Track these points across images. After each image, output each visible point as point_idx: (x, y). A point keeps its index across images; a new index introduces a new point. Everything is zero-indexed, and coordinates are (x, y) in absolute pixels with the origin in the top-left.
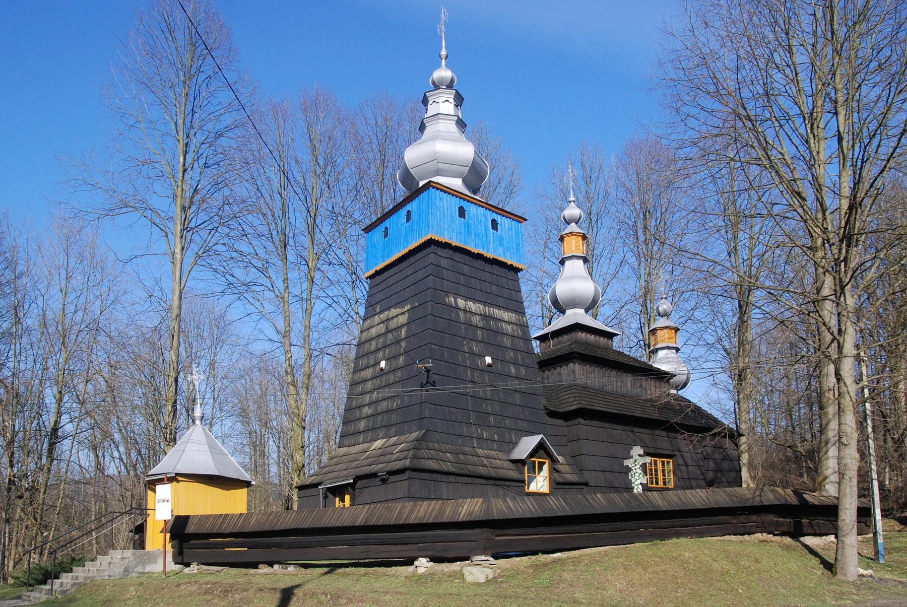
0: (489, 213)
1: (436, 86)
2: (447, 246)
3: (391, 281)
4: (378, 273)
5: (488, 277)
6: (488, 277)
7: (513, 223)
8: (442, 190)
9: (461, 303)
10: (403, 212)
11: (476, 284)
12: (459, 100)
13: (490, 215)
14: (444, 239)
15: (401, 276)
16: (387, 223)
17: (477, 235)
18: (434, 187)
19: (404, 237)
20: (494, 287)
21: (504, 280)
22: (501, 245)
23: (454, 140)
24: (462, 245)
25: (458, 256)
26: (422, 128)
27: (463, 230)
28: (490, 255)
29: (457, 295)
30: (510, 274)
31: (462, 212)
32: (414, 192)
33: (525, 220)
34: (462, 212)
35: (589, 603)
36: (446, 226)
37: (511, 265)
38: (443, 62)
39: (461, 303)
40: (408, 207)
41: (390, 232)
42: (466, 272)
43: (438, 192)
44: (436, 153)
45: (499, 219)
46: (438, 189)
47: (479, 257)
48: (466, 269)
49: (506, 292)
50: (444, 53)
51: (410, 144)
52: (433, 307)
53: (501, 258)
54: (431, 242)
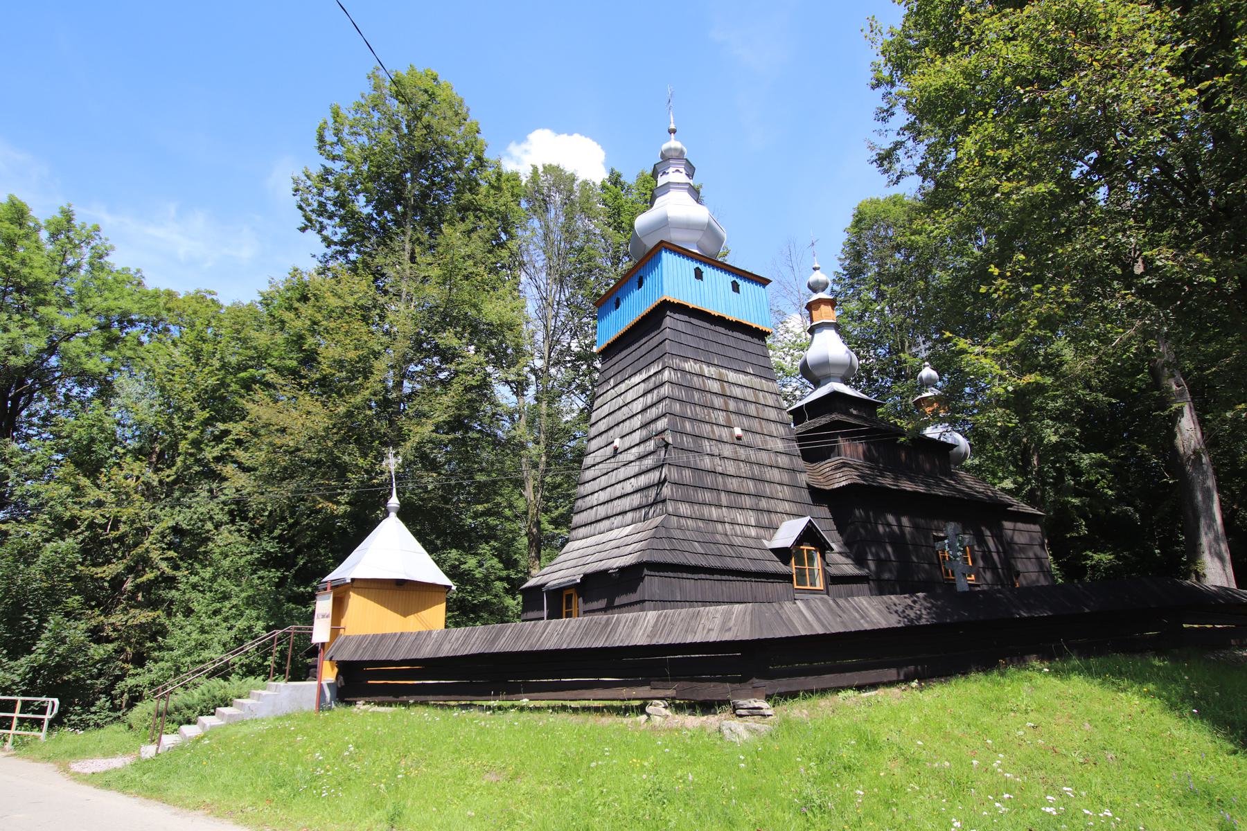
34: (699, 274)
44: (667, 218)
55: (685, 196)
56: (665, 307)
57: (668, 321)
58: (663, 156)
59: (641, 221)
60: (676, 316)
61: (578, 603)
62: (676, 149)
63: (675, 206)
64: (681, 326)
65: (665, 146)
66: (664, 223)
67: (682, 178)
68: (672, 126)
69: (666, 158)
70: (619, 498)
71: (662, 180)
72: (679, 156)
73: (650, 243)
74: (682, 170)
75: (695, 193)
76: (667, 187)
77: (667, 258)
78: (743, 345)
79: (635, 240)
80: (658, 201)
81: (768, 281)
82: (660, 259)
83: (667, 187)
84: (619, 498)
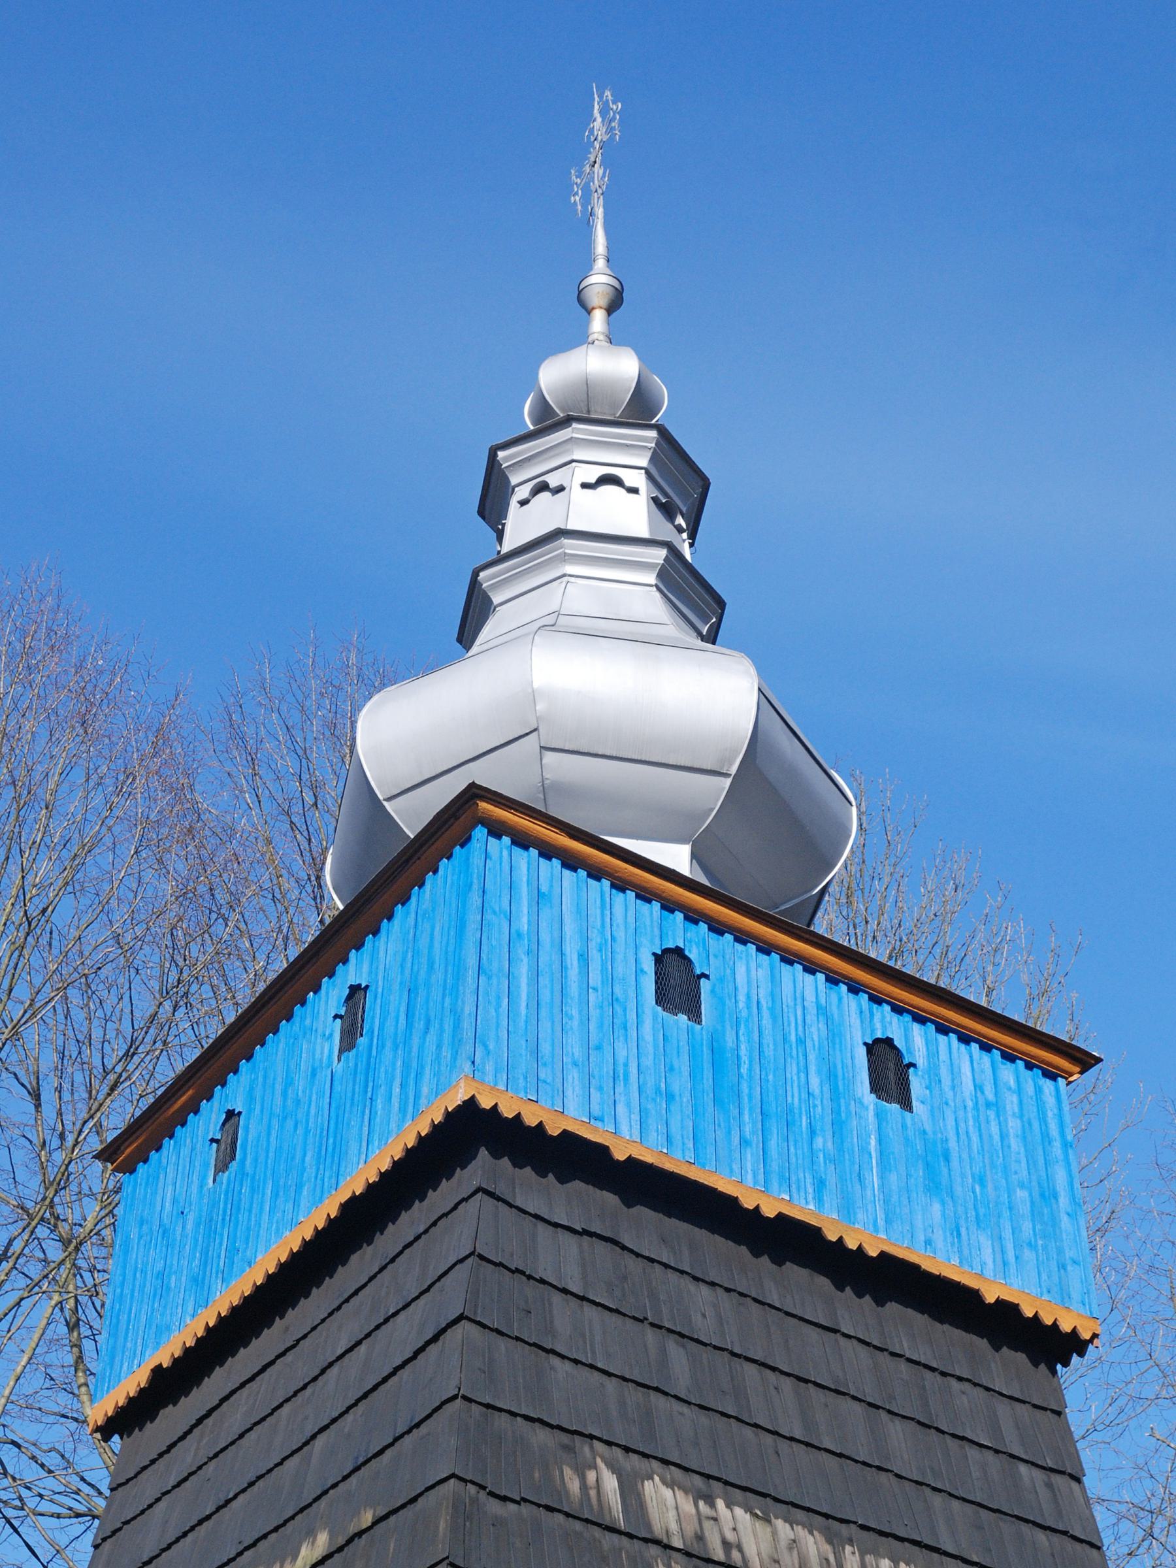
0: (852, 1006)
1: (549, 420)
2: (574, 1158)
3: (235, 1416)
4: (168, 1385)
5: (856, 1367)
6: (856, 1367)
7: (1010, 1073)
8: (547, 852)
9: (668, 1505)
10: (329, 998)
11: (783, 1406)
12: (681, 486)
13: (859, 1020)
14: (563, 1111)
15: (299, 1367)
16: (235, 1092)
17: (765, 1094)
18: (497, 830)
19: (322, 1124)
20: (896, 1431)
21: (965, 1398)
22: (934, 1186)
23: (639, 639)
24: (678, 1160)
25: (646, 1228)
26: (475, 611)
27: (680, 1084)
28: (865, 1231)
29: (640, 1454)
30: (1007, 1367)
31: (677, 983)
32: (394, 871)
33: (1085, 1061)
34: (677, 983)
35: (5, 734)
36: (575, 1048)
37: (1007, 1310)
38: (599, 316)
39: (668, 1505)
40: (354, 970)
41: (249, 1132)
42: (705, 1328)
43: (526, 859)
44: (533, 696)
45: (915, 1041)
46: (522, 841)
47: (791, 1241)
48: (703, 1310)
49: (979, 1473)
50: (599, 280)
51: (384, 686)
52: (463, 1514)
53: (941, 1260)
54: (470, 1132)
75: (697, 601)
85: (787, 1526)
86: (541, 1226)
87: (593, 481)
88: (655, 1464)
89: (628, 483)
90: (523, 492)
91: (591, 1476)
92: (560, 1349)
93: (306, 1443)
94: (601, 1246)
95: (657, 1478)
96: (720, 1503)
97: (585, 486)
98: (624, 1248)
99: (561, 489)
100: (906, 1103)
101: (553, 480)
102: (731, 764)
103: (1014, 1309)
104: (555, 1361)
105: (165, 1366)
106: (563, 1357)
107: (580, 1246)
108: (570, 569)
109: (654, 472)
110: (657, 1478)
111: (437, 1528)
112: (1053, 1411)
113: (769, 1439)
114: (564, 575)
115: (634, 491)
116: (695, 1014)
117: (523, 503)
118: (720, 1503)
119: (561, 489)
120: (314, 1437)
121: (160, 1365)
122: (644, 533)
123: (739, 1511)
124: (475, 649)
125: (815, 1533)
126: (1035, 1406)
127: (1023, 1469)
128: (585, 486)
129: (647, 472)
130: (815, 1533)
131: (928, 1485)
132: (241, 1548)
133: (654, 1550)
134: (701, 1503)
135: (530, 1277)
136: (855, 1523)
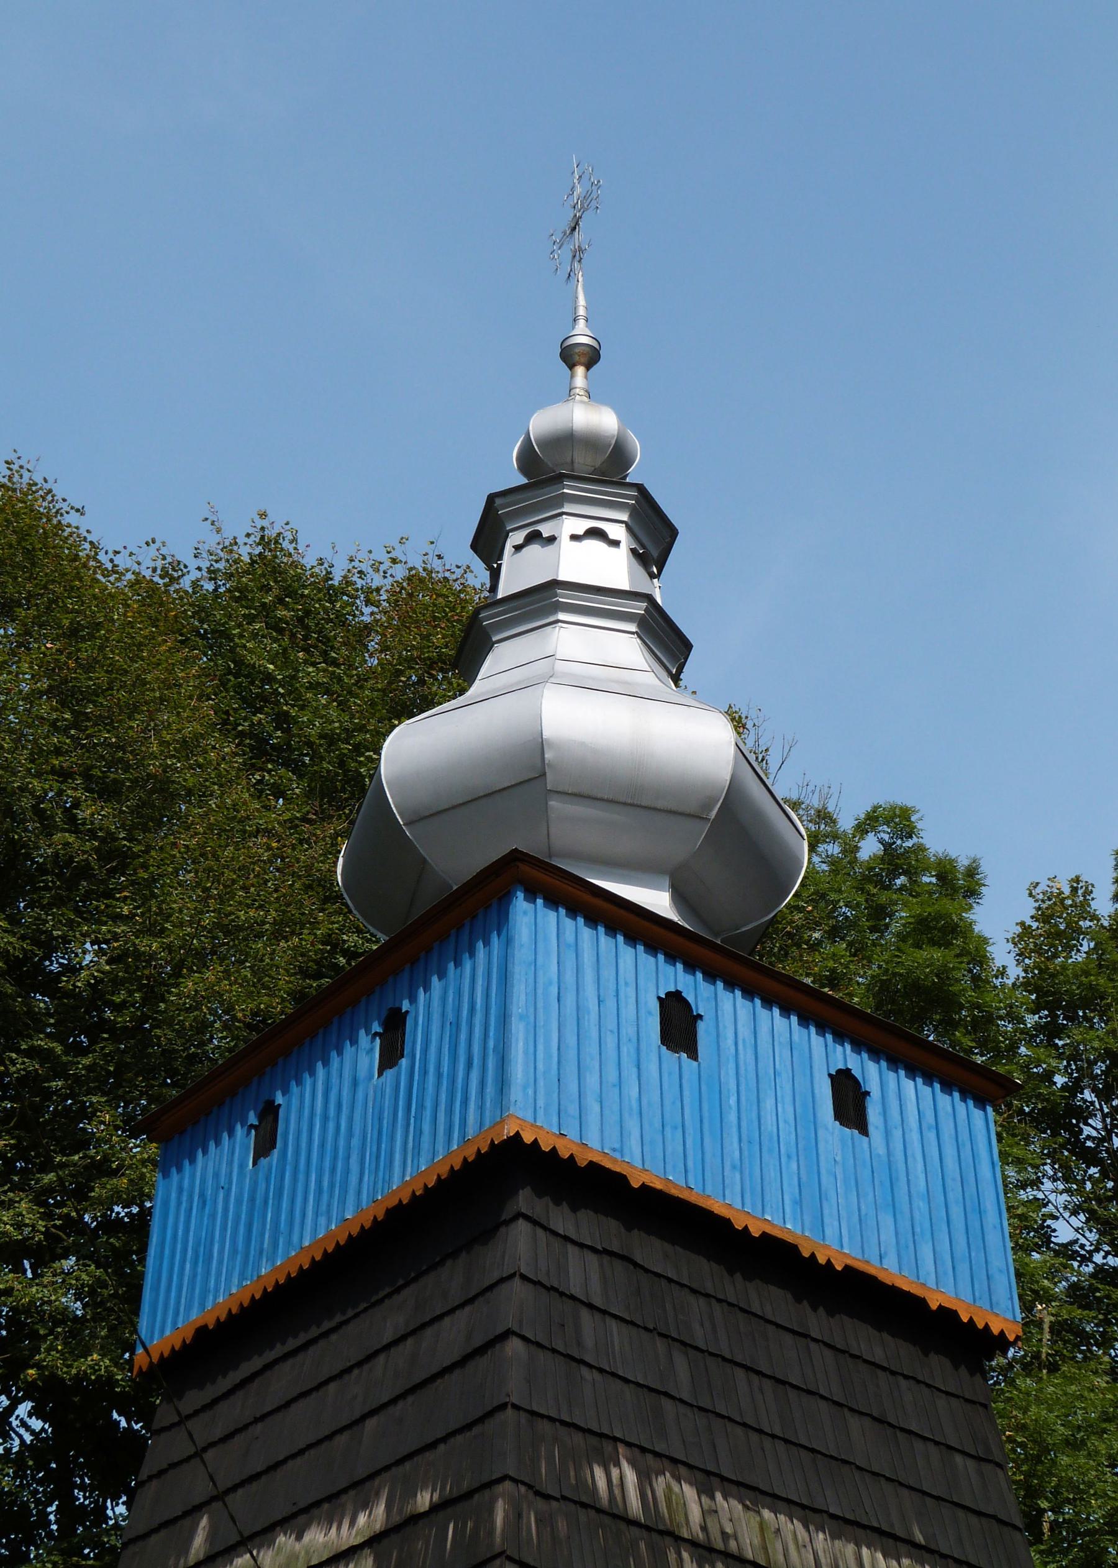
31: (679, 1026)
34: (679, 1026)
44: (540, 745)
55: (625, 648)
56: (511, 1173)
57: (520, 1245)
58: (529, 460)
59: (416, 750)
60: (562, 1220)
61: (584, 461)
62: (590, 442)
63: (579, 696)
64: (583, 1275)
65: (543, 422)
66: (529, 776)
67: (610, 565)
68: (582, 336)
69: (552, 472)
70: (348, 1370)
71: (520, 571)
72: (606, 467)
73: (458, 860)
74: (617, 532)
75: (668, 642)
76: (544, 601)
77: (532, 922)
78: (282, 1383)
79: (387, 844)
80: (503, 662)
81: (862, 1127)
82: (502, 920)
83: (544, 601)
84: (348, 1370)
85: (773, 1515)
86: (571, 1248)
87: (581, 533)
88: (666, 1463)
89: (612, 536)
90: (517, 538)
91: (615, 1472)
92: (588, 1359)
93: (317, 1388)
94: (618, 1265)
95: (668, 1474)
96: (719, 1496)
97: (574, 538)
98: (636, 1265)
99: (552, 539)
100: (863, 1129)
101: (546, 530)
102: (711, 810)
103: (954, 1314)
104: (585, 1371)
105: (211, 1327)
106: (590, 1366)
107: (601, 1265)
108: (562, 616)
109: (636, 529)
110: (668, 1474)
111: (493, 1522)
112: (982, 1404)
113: (754, 1437)
114: (558, 621)
115: (616, 543)
116: (693, 1055)
117: (518, 548)
118: (719, 1496)
119: (552, 539)
120: (364, 1418)
121: (206, 1326)
122: (626, 586)
123: (734, 1503)
124: (477, 688)
125: (795, 1521)
126: (967, 1400)
127: (959, 1459)
128: (574, 538)
129: (629, 528)
130: (795, 1521)
131: (884, 1476)
132: (295, 1509)
133: (668, 1540)
134: (703, 1498)
135: (562, 1294)
136: (826, 1512)
